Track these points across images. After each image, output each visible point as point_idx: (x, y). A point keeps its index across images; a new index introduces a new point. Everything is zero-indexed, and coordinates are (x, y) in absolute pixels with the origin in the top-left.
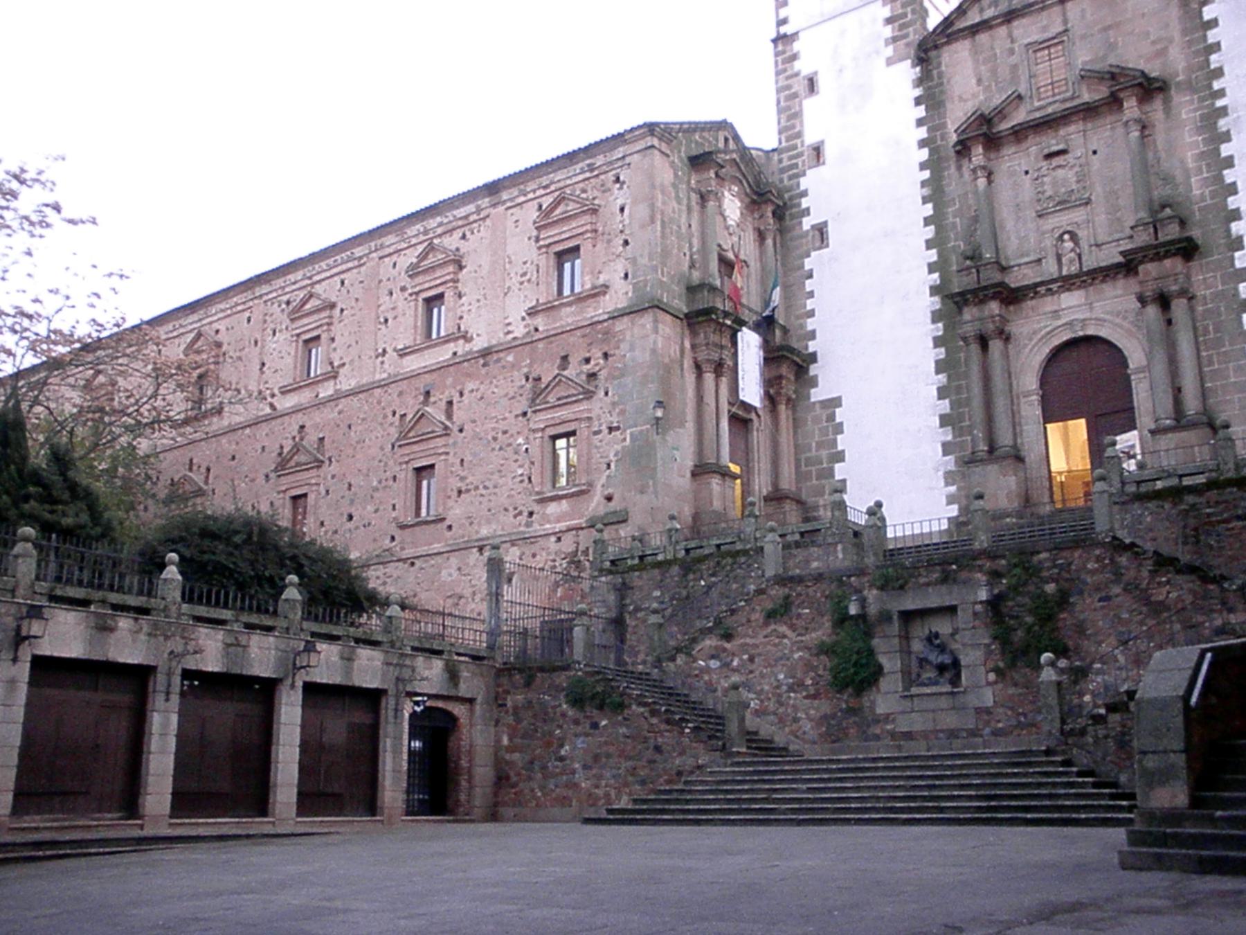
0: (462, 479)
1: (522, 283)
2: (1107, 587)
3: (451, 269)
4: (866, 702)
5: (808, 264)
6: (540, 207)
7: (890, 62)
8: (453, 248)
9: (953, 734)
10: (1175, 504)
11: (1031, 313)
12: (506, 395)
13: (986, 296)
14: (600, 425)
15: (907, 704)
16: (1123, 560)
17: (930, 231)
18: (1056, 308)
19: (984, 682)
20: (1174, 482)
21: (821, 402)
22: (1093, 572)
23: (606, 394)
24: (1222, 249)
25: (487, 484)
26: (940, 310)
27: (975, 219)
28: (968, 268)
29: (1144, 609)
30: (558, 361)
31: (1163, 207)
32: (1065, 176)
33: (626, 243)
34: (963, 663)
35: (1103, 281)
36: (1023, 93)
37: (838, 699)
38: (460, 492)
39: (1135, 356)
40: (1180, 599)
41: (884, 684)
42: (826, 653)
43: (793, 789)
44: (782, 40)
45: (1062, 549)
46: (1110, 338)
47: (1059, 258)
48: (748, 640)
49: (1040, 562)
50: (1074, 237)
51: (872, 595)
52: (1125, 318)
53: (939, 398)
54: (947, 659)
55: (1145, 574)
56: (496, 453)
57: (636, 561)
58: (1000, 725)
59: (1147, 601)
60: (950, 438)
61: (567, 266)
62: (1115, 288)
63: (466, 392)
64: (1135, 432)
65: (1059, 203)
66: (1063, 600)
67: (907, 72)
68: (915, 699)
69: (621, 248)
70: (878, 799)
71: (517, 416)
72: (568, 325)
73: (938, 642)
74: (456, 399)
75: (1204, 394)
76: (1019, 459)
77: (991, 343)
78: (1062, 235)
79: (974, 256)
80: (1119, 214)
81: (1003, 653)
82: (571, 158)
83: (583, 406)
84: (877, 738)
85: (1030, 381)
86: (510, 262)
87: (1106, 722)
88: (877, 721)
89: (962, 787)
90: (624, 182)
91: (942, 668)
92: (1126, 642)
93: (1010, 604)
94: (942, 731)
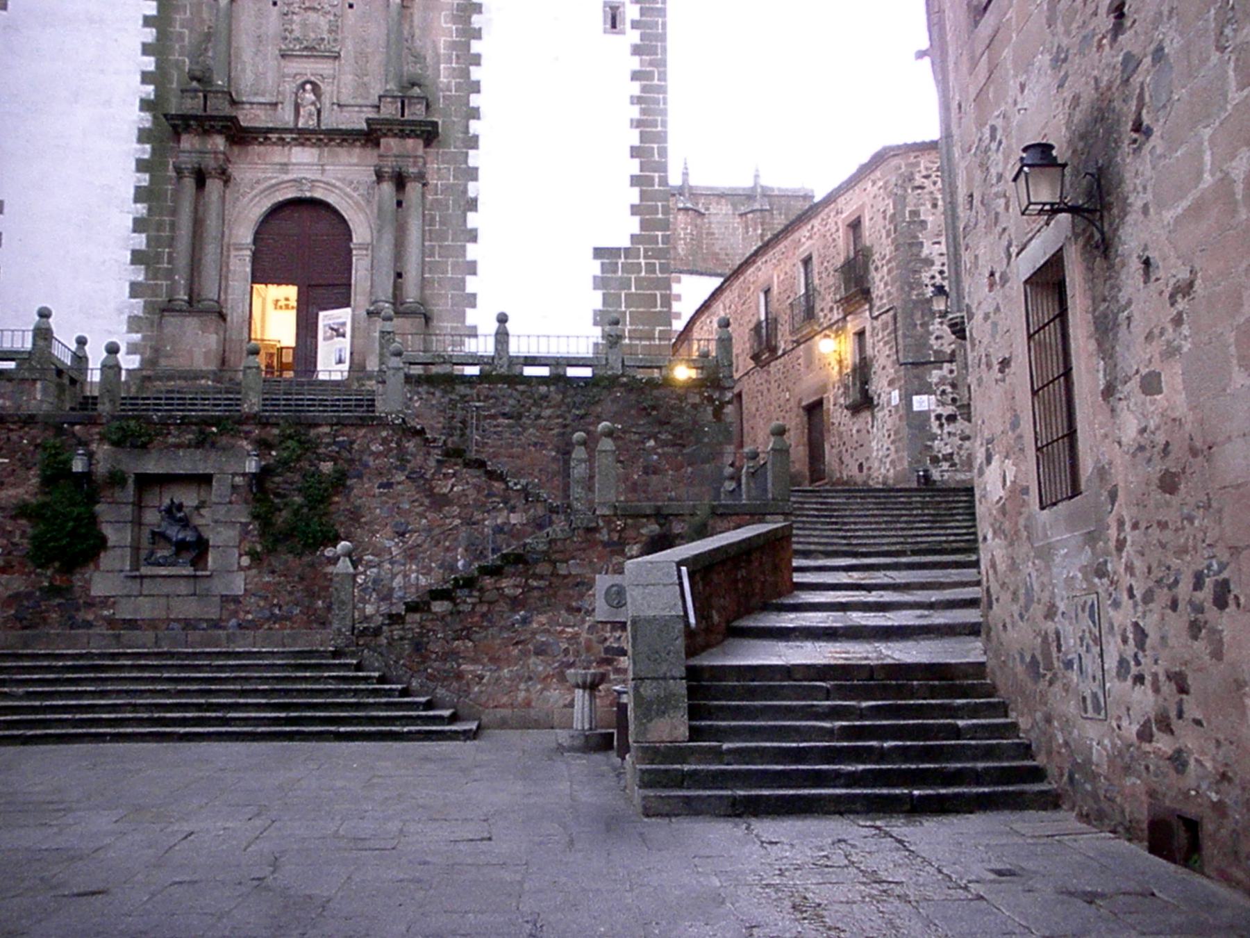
2: (389, 470)
4: (78, 581)
9: (188, 624)
10: (445, 392)
11: (256, 160)
13: (212, 127)
15: (134, 587)
16: (411, 445)
17: (150, 35)
18: (285, 160)
19: (236, 567)
22: (377, 455)
24: (458, 144)
26: (150, 130)
27: (208, 37)
28: (196, 91)
29: (427, 502)
31: (413, 85)
34: (211, 543)
35: (339, 145)
37: (37, 575)
39: (361, 233)
40: (464, 494)
41: (106, 560)
42: (29, 517)
45: (345, 425)
46: (338, 207)
47: (297, 107)
49: (318, 436)
50: (316, 89)
51: (103, 451)
53: (134, 231)
54: (190, 536)
55: (432, 463)
58: (250, 617)
59: (430, 493)
60: (141, 278)
62: (350, 156)
64: (349, 310)
65: (306, 48)
66: (339, 482)
68: (145, 580)
70: (135, 707)
73: (181, 514)
75: (424, 283)
76: (222, 317)
77: (209, 182)
78: (303, 86)
79: (202, 79)
80: (366, 79)
81: (262, 535)
84: (88, 625)
85: (244, 234)
87: (403, 623)
88: (90, 604)
89: (244, 693)
91: (181, 546)
92: (403, 535)
93: (277, 479)
94: (177, 620)
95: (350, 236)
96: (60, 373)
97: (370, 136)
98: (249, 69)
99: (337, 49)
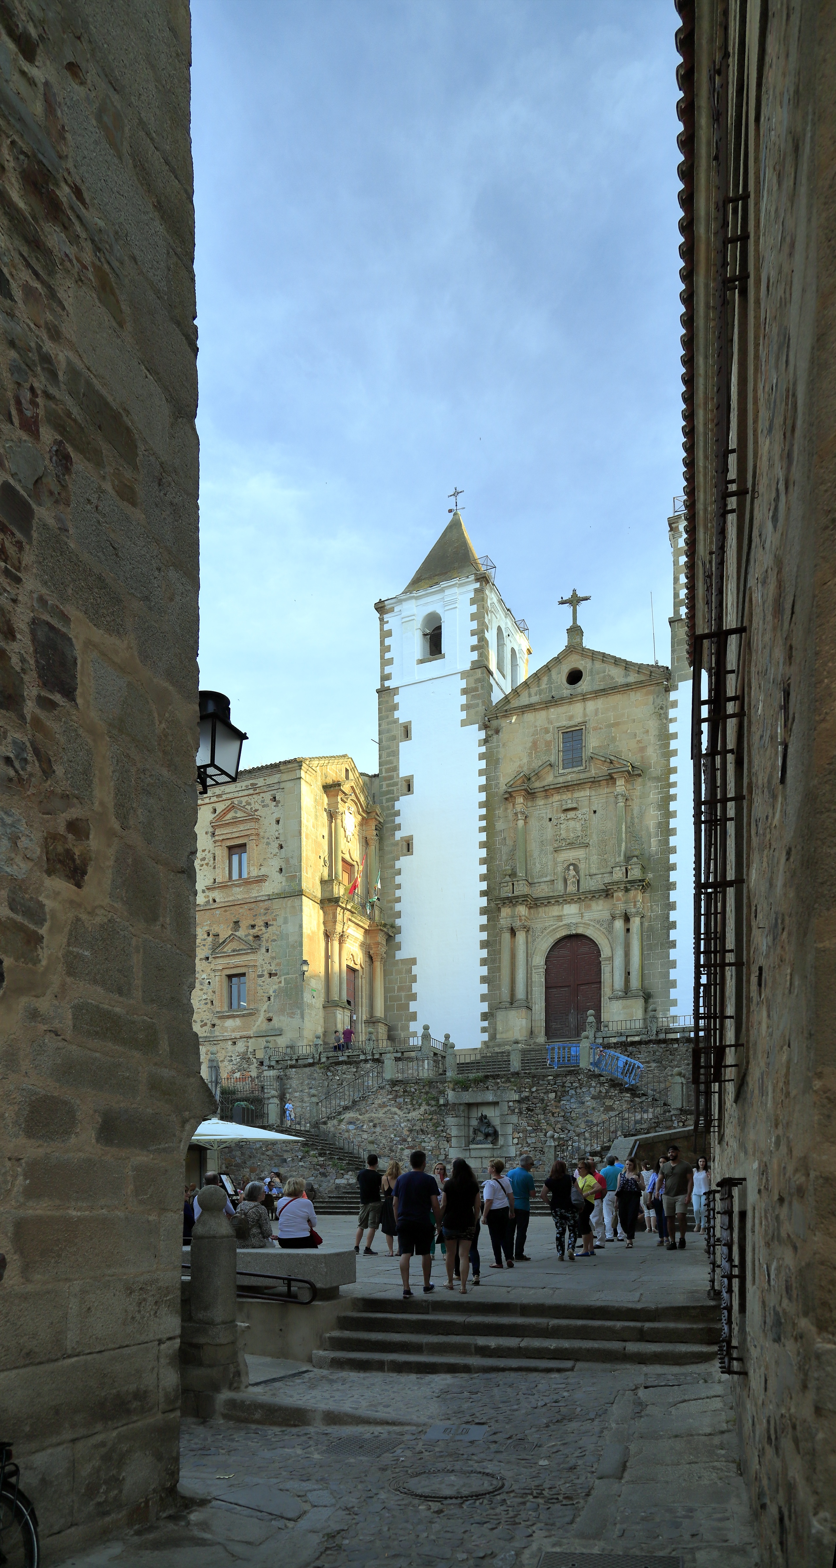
1: (202, 865)
5: (398, 865)
6: (215, 811)
7: (464, 723)
14: (263, 971)
17: (483, 853)
18: (561, 914)
20: (624, 1039)
21: (402, 960)
23: (267, 950)
30: (232, 925)
32: (571, 827)
33: (281, 847)
44: (385, 693)
47: (565, 881)
48: (373, 1115)
54: (490, 1130)
57: (294, 1062)
61: (235, 858)
69: (277, 850)
78: (568, 868)
83: (251, 957)
90: (279, 802)
95: (599, 952)
96: (435, 1054)
97: (607, 893)
98: (537, 861)
99: (587, 841)
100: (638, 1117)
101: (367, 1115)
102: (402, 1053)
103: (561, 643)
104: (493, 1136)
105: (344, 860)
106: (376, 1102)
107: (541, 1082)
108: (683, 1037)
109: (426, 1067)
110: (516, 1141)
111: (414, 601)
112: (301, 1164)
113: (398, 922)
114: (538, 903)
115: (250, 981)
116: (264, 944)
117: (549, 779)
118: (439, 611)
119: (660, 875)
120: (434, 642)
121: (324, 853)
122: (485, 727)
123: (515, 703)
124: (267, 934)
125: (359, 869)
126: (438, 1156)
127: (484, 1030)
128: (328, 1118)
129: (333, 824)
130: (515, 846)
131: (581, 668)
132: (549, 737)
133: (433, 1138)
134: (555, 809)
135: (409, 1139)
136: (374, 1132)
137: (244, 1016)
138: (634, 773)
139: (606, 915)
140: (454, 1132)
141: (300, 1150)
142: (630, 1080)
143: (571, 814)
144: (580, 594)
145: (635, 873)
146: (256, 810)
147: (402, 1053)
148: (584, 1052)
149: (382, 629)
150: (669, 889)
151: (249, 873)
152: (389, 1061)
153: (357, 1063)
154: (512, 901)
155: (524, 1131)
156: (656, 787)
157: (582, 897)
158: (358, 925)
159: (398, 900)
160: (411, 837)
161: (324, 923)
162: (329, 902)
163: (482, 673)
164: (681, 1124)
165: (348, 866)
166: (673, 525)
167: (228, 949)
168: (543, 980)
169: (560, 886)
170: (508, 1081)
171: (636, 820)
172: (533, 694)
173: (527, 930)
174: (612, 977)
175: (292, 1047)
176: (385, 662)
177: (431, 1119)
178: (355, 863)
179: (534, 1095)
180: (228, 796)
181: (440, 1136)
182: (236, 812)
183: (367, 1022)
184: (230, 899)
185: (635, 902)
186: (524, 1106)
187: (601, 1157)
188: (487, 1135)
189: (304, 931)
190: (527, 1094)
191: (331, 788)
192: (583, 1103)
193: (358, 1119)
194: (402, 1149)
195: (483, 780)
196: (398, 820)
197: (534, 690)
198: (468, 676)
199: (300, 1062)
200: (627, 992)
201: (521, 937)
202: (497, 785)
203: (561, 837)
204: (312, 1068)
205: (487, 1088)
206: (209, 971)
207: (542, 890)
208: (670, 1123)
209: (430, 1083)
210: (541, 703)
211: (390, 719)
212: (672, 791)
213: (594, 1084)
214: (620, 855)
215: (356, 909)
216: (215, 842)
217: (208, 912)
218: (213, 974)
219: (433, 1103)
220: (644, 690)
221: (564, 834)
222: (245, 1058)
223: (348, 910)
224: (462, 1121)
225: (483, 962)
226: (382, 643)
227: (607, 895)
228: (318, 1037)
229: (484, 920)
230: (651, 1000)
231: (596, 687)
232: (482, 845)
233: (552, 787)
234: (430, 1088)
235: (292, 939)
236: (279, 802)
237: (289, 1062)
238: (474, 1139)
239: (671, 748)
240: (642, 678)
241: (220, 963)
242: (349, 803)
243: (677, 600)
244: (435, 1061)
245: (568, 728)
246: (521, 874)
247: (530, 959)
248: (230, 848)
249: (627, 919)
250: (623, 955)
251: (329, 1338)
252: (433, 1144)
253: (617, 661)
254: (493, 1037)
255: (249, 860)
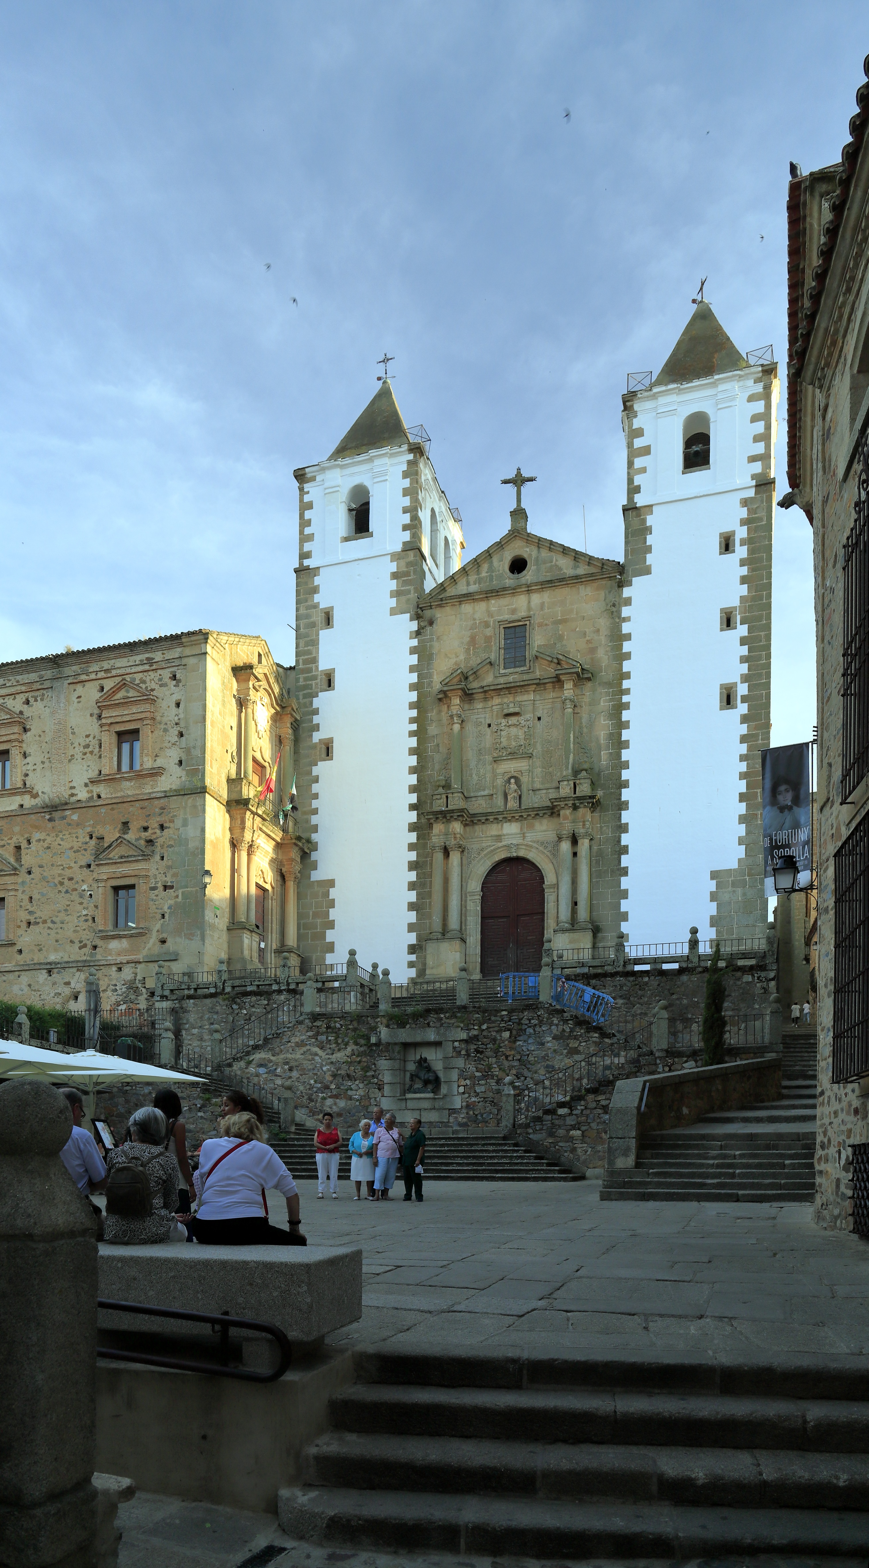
0: (31, 913)
3: (16, 729)
5: (315, 771)
6: (102, 689)
7: (393, 612)
8: (17, 710)
12: (72, 848)
14: (156, 883)
18: (500, 833)
23: (162, 858)
25: (54, 919)
30: (120, 826)
32: (513, 734)
36: (493, 661)
38: (29, 923)
43: (690, 1164)
44: (304, 573)
48: (289, 1056)
52: (546, 847)
54: (431, 1076)
56: (63, 894)
61: (126, 747)
63: (33, 840)
67: (406, 624)
69: (176, 739)
71: (81, 867)
72: (129, 796)
73: (426, 1065)
74: (24, 845)
78: (510, 778)
80: (551, 769)
82: (132, 647)
86: (73, 733)
90: (180, 681)
95: (542, 878)
96: (362, 986)
97: (552, 811)
98: (474, 772)
99: (531, 751)
100: (608, 1061)
101: (282, 1056)
102: (323, 982)
103: (503, 526)
104: (433, 1083)
105: (255, 760)
106: (293, 1040)
107: (493, 1018)
108: (655, 970)
109: (353, 1000)
110: (461, 1089)
111: (338, 470)
112: (200, 1114)
113: (314, 837)
114: (475, 820)
115: (141, 893)
116: (158, 850)
117: (489, 679)
118: (368, 483)
119: (611, 793)
120: (361, 520)
121: (232, 747)
122: (417, 617)
123: (451, 591)
124: (162, 838)
125: (272, 774)
126: (367, 1107)
127: (411, 965)
128: (234, 1059)
129: (243, 715)
130: (449, 754)
131: (526, 556)
132: (489, 632)
133: (361, 1085)
134: (495, 713)
135: (333, 1086)
136: (290, 1077)
137: (131, 936)
138: (583, 676)
139: (552, 836)
140: (387, 1078)
141: (199, 1097)
142: (598, 1019)
143: (513, 720)
144: (525, 474)
145: (584, 789)
146: (152, 690)
147: (323, 982)
148: (544, 984)
149: (301, 500)
150: (621, 809)
151: (141, 765)
152: (309, 990)
153: (268, 994)
154: (445, 816)
155: (472, 1077)
156: (608, 694)
157: (525, 815)
158: (268, 836)
159: (315, 812)
160: (331, 740)
161: (231, 829)
162: (236, 805)
163: (415, 556)
164: (667, 1069)
165: (259, 766)
166: (628, 404)
167: (115, 854)
168: (479, 908)
169: (499, 801)
170: (454, 1016)
171: (585, 730)
172: (472, 583)
173: (462, 850)
174: (557, 907)
175: (189, 975)
176: (305, 538)
177: (359, 1062)
178: (266, 764)
179: (485, 1033)
180: (119, 672)
181: (370, 1083)
182: (128, 692)
183: (278, 952)
184: (119, 795)
185: (584, 822)
186: (473, 1047)
187: (571, 1108)
188: (426, 1082)
189: (207, 835)
190: (476, 1033)
191: (242, 671)
192: (543, 1044)
193: (270, 1061)
194: (324, 1099)
195: (414, 678)
196: (316, 719)
197: (473, 578)
198: (399, 559)
199: (200, 992)
200: (574, 925)
201: (455, 857)
202: (430, 684)
203: (502, 746)
204: (214, 1000)
205: (428, 1024)
206: (90, 881)
207: (478, 806)
208: (654, 1067)
209: (359, 1018)
210: (481, 593)
211: (309, 603)
212: (625, 699)
213: (556, 1021)
214: (567, 768)
215: (268, 815)
216: (101, 726)
217: (91, 810)
218: (95, 885)
219: (362, 1042)
220: (595, 585)
221: (505, 742)
222: (132, 987)
223: (259, 816)
224: (397, 1064)
225: (412, 886)
226: (302, 516)
227: (552, 813)
228: (222, 962)
229: (413, 837)
230: (600, 935)
231: (542, 579)
232: (412, 751)
233: (492, 688)
234: (359, 1023)
235: (191, 845)
236: (180, 681)
237: (186, 992)
238: (411, 1086)
239: (624, 651)
240: (592, 570)
241: (105, 872)
242: (262, 693)
243: (631, 486)
244: (361, 994)
245: (510, 622)
246: (456, 786)
247: (464, 884)
248: (120, 734)
249: (574, 841)
250: (570, 882)
251: (318, 1459)
252: (361, 1092)
253: (565, 550)
254: (421, 973)
255: (142, 749)
